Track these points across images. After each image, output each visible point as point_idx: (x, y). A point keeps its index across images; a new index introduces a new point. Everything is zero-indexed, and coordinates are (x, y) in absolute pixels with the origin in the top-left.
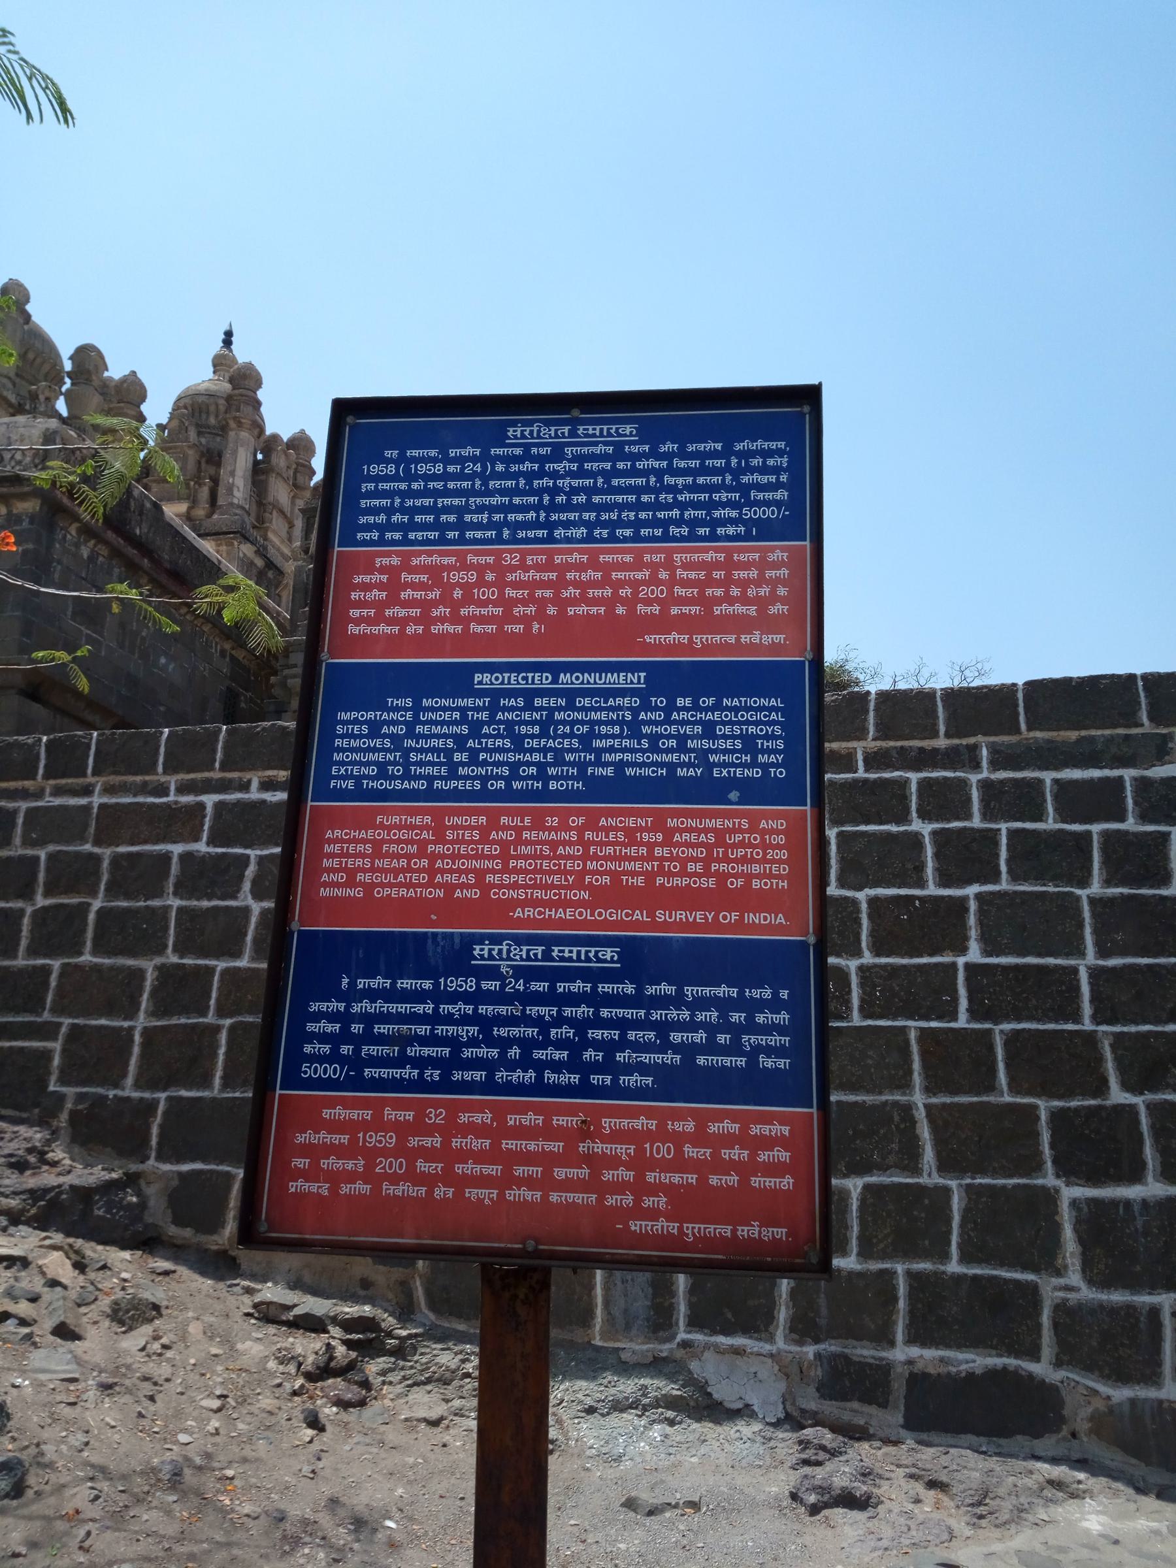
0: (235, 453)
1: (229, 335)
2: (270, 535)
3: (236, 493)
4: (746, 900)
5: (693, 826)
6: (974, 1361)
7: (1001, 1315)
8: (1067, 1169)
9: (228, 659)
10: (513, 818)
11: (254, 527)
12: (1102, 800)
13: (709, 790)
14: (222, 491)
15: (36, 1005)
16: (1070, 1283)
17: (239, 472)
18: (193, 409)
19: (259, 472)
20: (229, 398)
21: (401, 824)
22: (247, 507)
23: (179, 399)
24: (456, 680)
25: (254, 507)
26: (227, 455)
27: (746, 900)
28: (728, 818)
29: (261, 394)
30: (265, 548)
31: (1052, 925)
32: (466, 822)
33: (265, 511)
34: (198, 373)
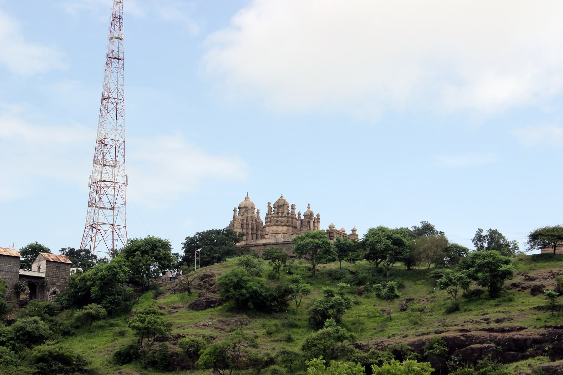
19: (314, 222)
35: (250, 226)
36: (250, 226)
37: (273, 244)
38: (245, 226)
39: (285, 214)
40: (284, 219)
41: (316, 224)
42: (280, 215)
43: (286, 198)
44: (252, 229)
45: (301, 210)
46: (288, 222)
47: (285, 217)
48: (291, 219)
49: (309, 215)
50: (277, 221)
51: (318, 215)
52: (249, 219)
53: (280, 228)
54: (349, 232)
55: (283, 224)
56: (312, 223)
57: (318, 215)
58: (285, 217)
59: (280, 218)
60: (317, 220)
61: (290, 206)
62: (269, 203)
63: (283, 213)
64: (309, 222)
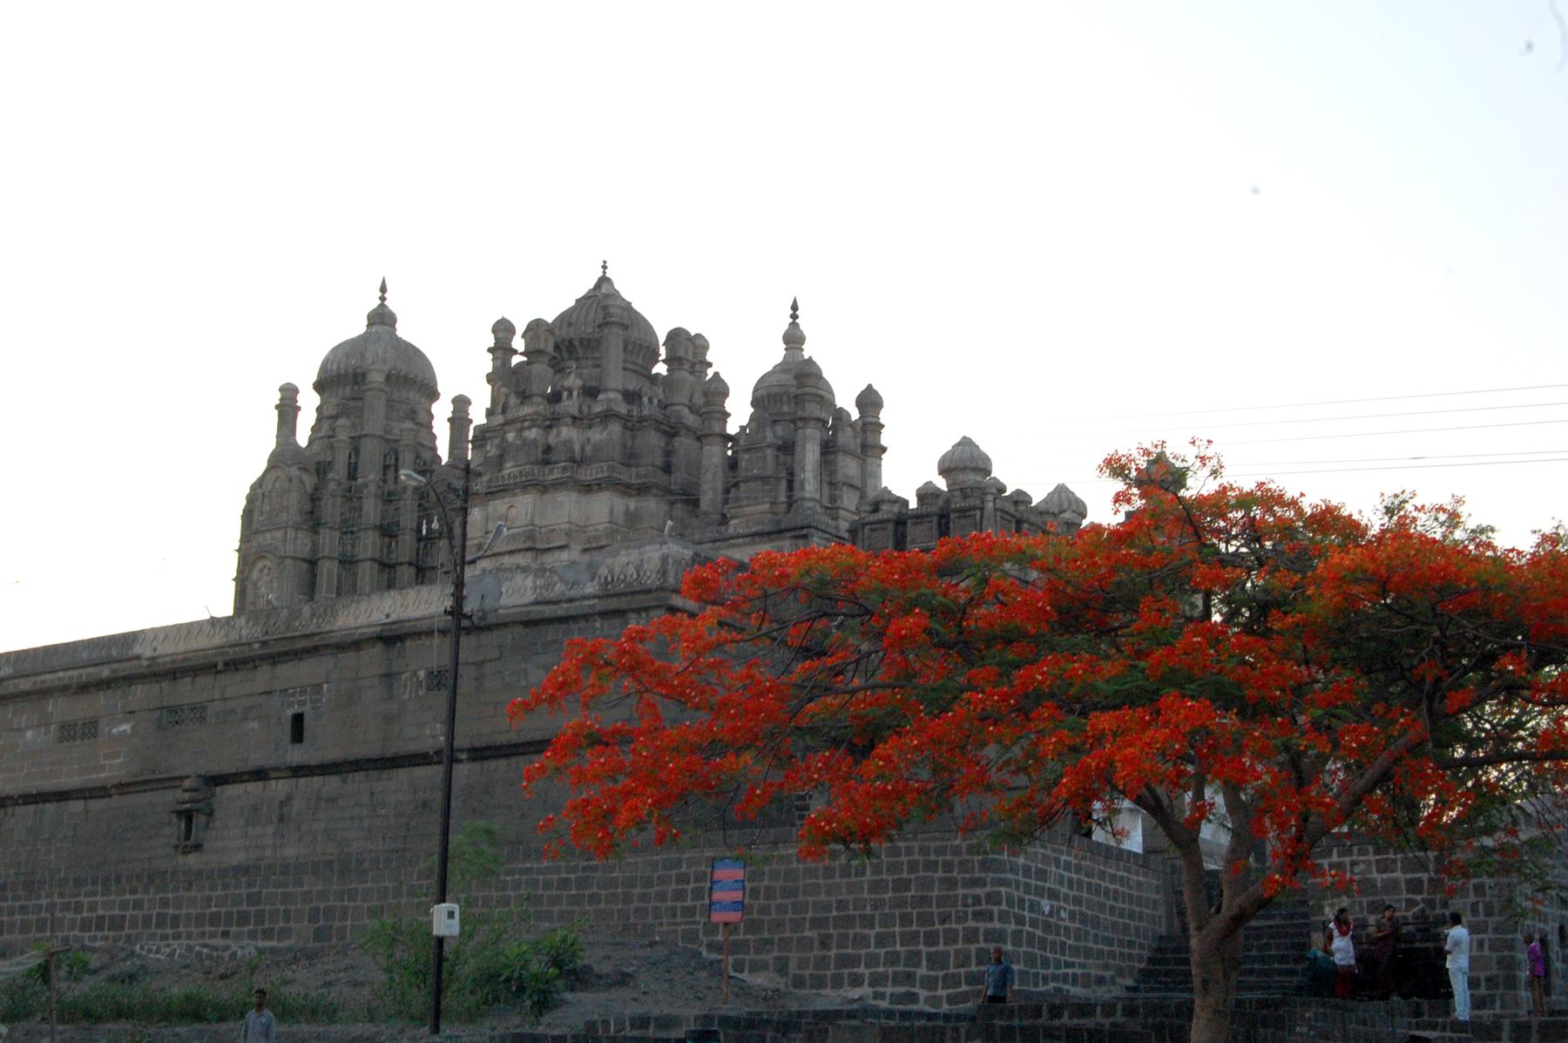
0: (804, 448)
1: (795, 307)
6: (903, 989)
7: (909, 978)
8: (926, 944)
12: (940, 851)
14: (797, 485)
15: (694, 915)
16: (922, 971)
17: (809, 467)
19: (829, 449)
23: (756, 390)
25: (826, 488)
26: (798, 449)
31: (926, 884)
34: (776, 353)
35: (371, 509)
36: (371, 509)
37: (123, 788)
38: (332, 509)
39: (611, 398)
40: (597, 435)
41: (848, 467)
42: (570, 405)
43: (634, 291)
44: (388, 531)
45: (884, 441)
46: (630, 457)
47: (608, 416)
48: (653, 440)
49: (794, 390)
50: (547, 456)
51: (869, 401)
52: (371, 455)
53: (566, 508)
54: (1375, 521)
55: (587, 474)
56: (810, 454)
57: (869, 401)
58: (608, 416)
59: (566, 432)
60: (863, 434)
61: (662, 338)
62: (503, 329)
63: (591, 392)
64: (787, 448)
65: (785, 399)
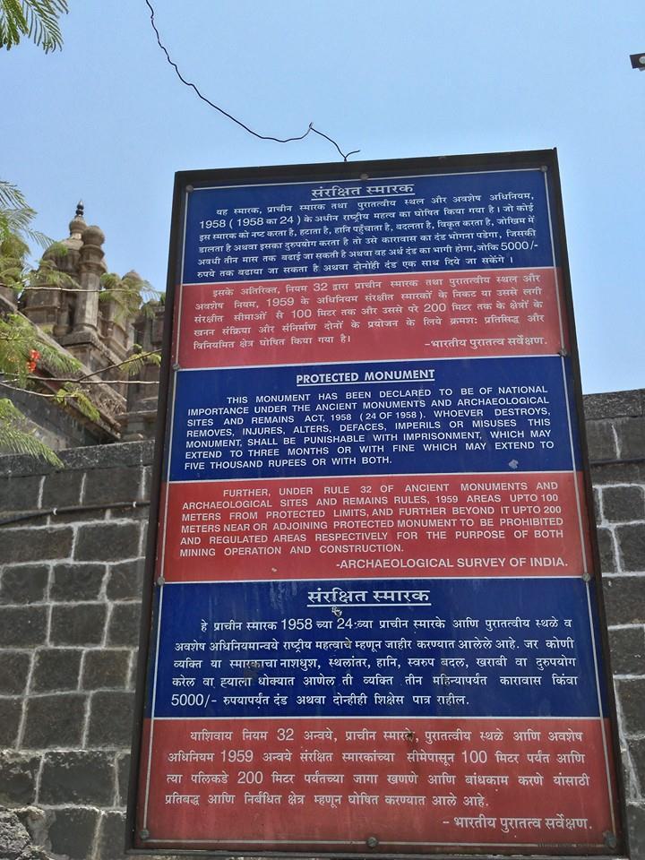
2: (112, 344)
3: (87, 315)
4: (528, 547)
5: (483, 488)
9: (83, 431)
10: (334, 487)
11: (101, 339)
13: (494, 460)
14: (78, 314)
18: (58, 259)
19: (104, 306)
20: (82, 251)
21: (243, 496)
22: (95, 325)
24: (282, 380)
27: (528, 547)
28: (513, 481)
29: (104, 247)
30: (108, 353)
32: (295, 491)
33: (108, 327)
65: (70, 258)
